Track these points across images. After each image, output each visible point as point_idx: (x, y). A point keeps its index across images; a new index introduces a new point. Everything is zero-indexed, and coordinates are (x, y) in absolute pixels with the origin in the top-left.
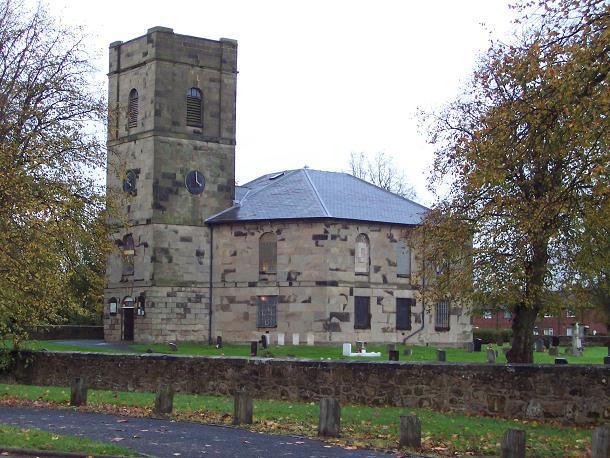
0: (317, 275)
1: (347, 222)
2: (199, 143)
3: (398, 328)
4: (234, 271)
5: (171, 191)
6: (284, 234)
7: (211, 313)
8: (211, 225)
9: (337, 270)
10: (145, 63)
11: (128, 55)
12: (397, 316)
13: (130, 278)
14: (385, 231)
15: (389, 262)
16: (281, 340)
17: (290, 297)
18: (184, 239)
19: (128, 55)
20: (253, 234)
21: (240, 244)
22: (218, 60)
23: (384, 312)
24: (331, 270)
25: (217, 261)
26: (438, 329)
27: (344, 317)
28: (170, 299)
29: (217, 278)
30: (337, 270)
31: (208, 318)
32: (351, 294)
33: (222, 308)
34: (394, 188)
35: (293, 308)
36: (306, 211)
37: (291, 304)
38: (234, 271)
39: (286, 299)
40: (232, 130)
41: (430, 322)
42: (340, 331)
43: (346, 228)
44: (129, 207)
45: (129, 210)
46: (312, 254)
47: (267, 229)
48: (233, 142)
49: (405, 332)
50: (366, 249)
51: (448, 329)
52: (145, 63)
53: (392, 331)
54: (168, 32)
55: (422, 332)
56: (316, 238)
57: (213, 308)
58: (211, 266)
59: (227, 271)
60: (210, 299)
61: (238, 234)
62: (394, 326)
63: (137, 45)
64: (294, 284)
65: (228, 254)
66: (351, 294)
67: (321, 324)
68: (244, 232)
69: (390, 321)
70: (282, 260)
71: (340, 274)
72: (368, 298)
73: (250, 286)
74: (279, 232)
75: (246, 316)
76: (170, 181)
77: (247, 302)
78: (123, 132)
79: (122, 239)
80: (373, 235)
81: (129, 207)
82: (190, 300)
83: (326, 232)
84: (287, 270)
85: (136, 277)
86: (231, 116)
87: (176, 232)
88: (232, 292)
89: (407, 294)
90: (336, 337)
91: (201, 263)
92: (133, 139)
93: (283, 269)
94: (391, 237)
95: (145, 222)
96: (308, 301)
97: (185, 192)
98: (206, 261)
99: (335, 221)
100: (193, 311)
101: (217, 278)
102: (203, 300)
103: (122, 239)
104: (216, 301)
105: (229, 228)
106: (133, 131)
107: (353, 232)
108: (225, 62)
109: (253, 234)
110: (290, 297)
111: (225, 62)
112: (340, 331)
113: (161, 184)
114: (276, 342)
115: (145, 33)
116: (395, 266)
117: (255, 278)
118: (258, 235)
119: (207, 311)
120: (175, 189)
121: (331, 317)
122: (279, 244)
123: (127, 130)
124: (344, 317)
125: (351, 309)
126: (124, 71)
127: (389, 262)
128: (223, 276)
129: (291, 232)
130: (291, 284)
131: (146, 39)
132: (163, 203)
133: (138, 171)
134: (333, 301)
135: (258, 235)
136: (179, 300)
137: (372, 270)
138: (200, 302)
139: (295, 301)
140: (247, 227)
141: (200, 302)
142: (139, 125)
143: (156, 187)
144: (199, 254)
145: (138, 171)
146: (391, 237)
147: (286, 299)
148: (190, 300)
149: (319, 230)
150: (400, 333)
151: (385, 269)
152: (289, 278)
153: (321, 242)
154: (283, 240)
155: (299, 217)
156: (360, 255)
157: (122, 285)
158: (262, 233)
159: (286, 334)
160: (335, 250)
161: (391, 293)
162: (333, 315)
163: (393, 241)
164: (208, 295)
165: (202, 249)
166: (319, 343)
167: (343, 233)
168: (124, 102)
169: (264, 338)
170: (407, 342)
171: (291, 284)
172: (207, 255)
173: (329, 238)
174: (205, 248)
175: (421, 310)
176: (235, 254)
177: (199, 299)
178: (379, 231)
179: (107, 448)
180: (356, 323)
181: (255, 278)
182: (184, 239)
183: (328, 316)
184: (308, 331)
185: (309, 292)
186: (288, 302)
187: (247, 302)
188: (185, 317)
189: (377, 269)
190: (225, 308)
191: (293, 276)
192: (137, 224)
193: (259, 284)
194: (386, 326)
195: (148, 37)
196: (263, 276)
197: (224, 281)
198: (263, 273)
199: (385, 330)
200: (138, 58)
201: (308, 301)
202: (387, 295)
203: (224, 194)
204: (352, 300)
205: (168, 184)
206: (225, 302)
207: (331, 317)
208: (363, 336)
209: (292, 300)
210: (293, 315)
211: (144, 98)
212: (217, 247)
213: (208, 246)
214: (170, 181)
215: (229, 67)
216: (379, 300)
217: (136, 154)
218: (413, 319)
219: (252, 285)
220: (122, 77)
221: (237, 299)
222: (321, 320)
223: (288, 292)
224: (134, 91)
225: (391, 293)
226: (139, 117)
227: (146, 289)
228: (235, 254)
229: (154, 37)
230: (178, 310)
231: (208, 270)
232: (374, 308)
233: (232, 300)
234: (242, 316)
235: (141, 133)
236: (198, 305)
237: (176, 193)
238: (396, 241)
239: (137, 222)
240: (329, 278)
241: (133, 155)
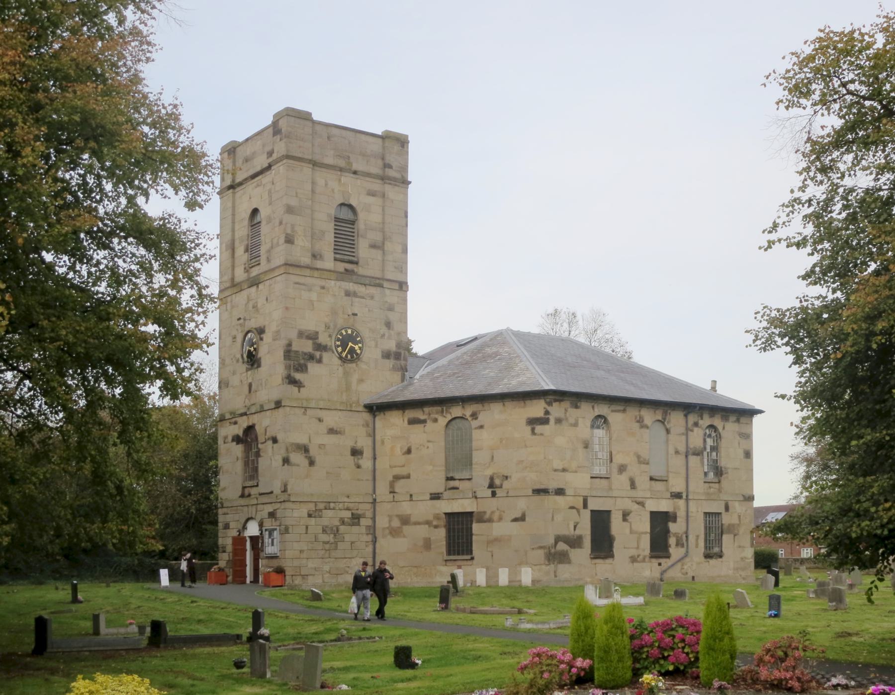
0: (534, 479)
1: (577, 398)
2: (351, 286)
3: (652, 557)
4: (408, 477)
5: (311, 357)
6: (483, 417)
7: (374, 541)
8: (375, 409)
9: (564, 470)
10: (269, 167)
11: (247, 160)
12: (449, 531)
13: (254, 491)
14: (632, 412)
15: (639, 457)
16: (481, 578)
17: (493, 512)
18: (332, 431)
19: (247, 160)
20: (436, 420)
21: (417, 435)
22: (380, 162)
23: (631, 532)
24: (556, 470)
25: (383, 463)
26: (708, 556)
27: (575, 542)
28: (312, 521)
29: (382, 489)
30: (564, 470)
31: (370, 549)
32: (585, 506)
33: (391, 533)
34: (808, 50)
35: (498, 529)
36: (514, 382)
37: (494, 524)
38: (408, 477)
39: (487, 516)
40: (402, 267)
41: (697, 546)
42: (569, 562)
43: (577, 407)
44: (250, 385)
45: (250, 391)
46: (526, 446)
47: (457, 411)
48: (402, 286)
49: (662, 561)
50: (606, 440)
51: (720, 556)
52: (269, 167)
53: (644, 561)
54: (304, 117)
55: (687, 560)
56: (533, 422)
57: (378, 533)
58: (374, 471)
59: (397, 478)
60: (374, 519)
61: (413, 422)
62: (647, 552)
63: (258, 145)
64: (499, 492)
65: (398, 451)
66: (585, 506)
67: (541, 552)
68: (422, 417)
69: (642, 546)
70: (478, 457)
71: (569, 476)
72: (608, 512)
73: (432, 499)
74: (474, 416)
75: (427, 544)
76: (310, 342)
77: (428, 523)
78: (240, 275)
79: (241, 434)
80: (616, 418)
81: (250, 385)
82: (343, 522)
83: (547, 412)
84: (489, 472)
85: (261, 489)
86: (399, 248)
87: (320, 420)
88: (406, 508)
89: (664, 506)
90: (565, 572)
91: (359, 467)
92: (255, 282)
93: (481, 474)
94: (640, 421)
95: (273, 406)
96: (522, 518)
97: (331, 359)
98: (366, 462)
99: (559, 396)
100: (347, 538)
101: (382, 489)
102: (363, 522)
103: (241, 434)
104: (382, 522)
105: (400, 412)
106: (255, 272)
107: (587, 412)
108: (390, 167)
109: (436, 420)
110: (493, 512)
111: (390, 167)
112: (569, 562)
113: (295, 347)
114: (473, 583)
115: (269, 121)
116: (648, 464)
117: (439, 485)
118: (442, 421)
119: (369, 538)
120: (317, 354)
121: (556, 543)
122: (476, 434)
123: (247, 270)
124: (575, 542)
125: (585, 530)
126: (240, 184)
127: (639, 457)
128: (392, 485)
129: (493, 414)
130: (494, 494)
131: (271, 130)
132: (298, 376)
133: (261, 331)
134: (559, 518)
135: (442, 421)
136: (325, 521)
137: (615, 470)
138: (358, 524)
139: (500, 519)
140: (426, 410)
141: (358, 524)
142: (263, 259)
143: (288, 353)
144: (356, 452)
145: (261, 331)
146: (640, 421)
147: (487, 516)
148: (343, 522)
149: (537, 409)
150: (655, 562)
151: (634, 470)
152: (491, 485)
153: (539, 428)
154: (481, 427)
155: (506, 391)
156: (597, 448)
157: (243, 502)
158: (449, 417)
159: (487, 569)
160: (560, 441)
161: (642, 504)
162: (558, 539)
163: (644, 426)
164: (369, 514)
165: (359, 445)
166: (539, 581)
167: (573, 413)
168: (242, 230)
169: (454, 578)
170: (667, 576)
171: (494, 494)
172: (368, 453)
173: (552, 421)
174: (364, 443)
175: (684, 529)
176: (409, 451)
177: (356, 519)
178: (624, 411)
179: (876, 299)
180: (592, 551)
181: (439, 485)
182: (332, 431)
183: (552, 541)
184: (521, 564)
185: (522, 505)
186: (490, 520)
187: (428, 523)
188: (336, 548)
189: (622, 469)
190: (395, 532)
191: (497, 482)
192: (262, 410)
193: (446, 495)
194: (634, 552)
195: (275, 128)
196: (452, 484)
197: (392, 492)
198: (452, 479)
199: (634, 559)
200: (261, 162)
201: (522, 518)
202: (636, 506)
203: (390, 363)
204: (586, 516)
205: (307, 347)
206: (396, 523)
207: (556, 543)
208: (603, 568)
209: (496, 517)
210: (497, 540)
211: (269, 220)
212: (383, 442)
213: (369, 441)
214: (310, 342)
215: (397, 175)
216: (625, 515)
217: (259, 305)
218: (672, 541)
219: (436, 497)
220: (238, 195)
221: (413, 519)
222: (541, 548)
223: (489, 506)
224: (255, 211)
225: (642, 504)
226: (263, 249)
227: (277, 506)
228: (409, 451)
229: (283, 124)
230: (324, 537)
231: (370, 477)
232: (617, 527)
233: (405, 520)
234: (421, 543)
235: (266, 272)
236: (355, 529)
237: (320, 361)
238: (647, 427)
239: (262, 406)
240: (552, 485)
241: (255, 307)
